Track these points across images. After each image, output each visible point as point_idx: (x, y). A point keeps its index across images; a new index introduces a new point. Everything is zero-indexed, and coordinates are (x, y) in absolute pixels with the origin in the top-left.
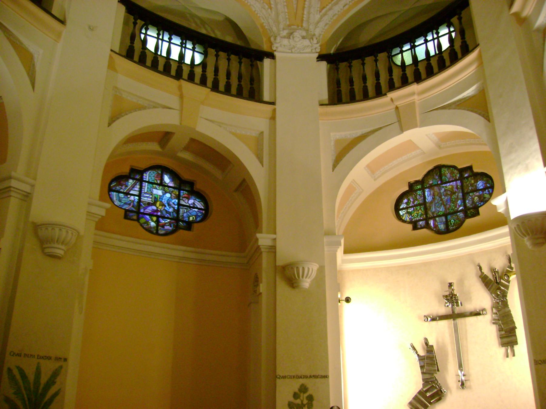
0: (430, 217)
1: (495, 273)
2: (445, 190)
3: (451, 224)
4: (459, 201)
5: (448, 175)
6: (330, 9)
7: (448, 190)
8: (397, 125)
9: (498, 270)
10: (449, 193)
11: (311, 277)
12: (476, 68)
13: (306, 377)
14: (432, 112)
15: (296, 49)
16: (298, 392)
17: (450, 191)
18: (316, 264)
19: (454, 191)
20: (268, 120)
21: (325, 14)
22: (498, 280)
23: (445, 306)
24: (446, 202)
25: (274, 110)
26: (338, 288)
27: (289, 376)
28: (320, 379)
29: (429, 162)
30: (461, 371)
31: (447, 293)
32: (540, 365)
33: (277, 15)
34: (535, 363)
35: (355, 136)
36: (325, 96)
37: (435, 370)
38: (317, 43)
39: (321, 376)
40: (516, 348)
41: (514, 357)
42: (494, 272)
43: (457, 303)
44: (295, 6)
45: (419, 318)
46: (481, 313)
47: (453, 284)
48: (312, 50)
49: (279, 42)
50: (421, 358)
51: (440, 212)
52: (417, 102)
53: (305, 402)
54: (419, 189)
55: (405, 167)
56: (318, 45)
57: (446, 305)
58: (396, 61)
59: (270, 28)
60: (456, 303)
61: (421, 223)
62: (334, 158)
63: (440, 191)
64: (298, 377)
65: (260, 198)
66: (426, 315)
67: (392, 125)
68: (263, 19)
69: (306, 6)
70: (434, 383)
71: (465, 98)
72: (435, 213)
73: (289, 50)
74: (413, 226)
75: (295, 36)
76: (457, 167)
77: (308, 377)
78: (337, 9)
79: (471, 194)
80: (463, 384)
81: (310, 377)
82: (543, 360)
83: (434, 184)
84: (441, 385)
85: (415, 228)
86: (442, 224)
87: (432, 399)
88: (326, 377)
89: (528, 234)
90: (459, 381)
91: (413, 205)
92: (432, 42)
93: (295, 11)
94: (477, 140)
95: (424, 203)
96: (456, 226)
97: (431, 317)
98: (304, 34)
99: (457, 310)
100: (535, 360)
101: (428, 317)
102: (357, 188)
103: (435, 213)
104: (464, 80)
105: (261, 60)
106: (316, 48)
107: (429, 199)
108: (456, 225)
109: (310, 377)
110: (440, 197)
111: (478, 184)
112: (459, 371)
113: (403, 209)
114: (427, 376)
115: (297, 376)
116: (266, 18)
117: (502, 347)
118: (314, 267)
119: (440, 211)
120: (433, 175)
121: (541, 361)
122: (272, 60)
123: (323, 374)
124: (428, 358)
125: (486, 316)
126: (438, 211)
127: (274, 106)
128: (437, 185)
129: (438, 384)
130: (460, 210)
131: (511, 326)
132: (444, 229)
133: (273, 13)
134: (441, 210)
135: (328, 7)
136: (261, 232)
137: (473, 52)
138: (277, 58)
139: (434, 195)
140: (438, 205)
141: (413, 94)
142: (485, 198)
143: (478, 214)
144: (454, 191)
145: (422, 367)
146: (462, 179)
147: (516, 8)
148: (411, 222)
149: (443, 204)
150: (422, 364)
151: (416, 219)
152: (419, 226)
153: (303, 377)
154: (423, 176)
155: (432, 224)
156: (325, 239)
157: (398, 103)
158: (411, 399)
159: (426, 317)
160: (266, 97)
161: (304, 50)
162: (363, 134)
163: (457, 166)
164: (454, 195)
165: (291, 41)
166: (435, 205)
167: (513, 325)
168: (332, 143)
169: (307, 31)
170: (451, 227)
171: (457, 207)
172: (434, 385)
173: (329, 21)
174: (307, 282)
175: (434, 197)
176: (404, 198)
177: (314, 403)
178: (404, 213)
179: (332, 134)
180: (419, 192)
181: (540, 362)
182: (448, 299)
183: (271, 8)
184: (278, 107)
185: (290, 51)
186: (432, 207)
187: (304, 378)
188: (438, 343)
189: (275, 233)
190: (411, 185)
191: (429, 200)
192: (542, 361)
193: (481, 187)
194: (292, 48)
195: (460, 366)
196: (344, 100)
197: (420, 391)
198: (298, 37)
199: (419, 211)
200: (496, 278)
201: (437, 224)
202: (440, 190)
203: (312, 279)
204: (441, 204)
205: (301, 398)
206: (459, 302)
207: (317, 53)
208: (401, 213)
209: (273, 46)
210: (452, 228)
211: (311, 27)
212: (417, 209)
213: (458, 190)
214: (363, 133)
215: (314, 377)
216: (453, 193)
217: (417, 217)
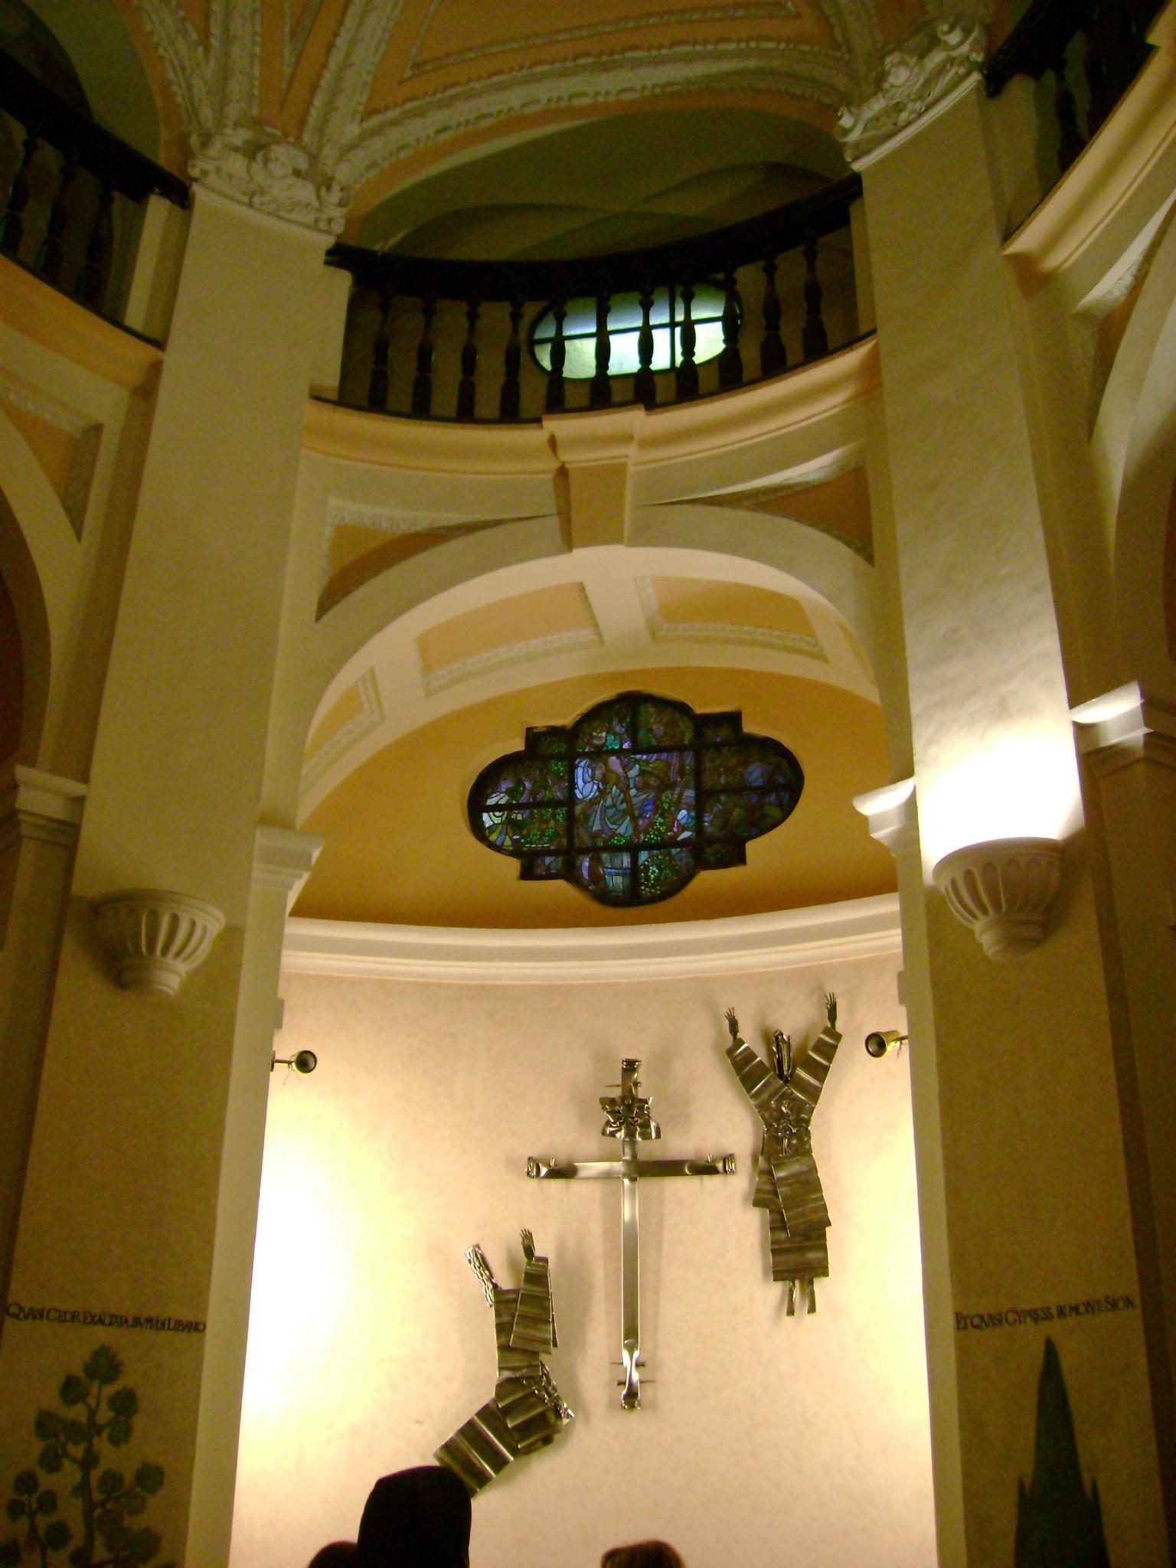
0: (584, 846)
1: (778, 1047)
2: (642, 773)
3: (648, 878)
4: (684, 812)
5: (659, 729)
6: (396, 123)
7: (651, 773)
8: (553, 523)
9: (789, 1038)
10: (652, 782)
11: (192, 958)
12: (847, 401)
13: (119, 1321)
14: (677, 507)
15: (266, 198)
16: (82, 1375)
17: (658, 777)
18: (220, 915)
19: (672, 780)
20: (126, 394)
21: (377, 132)
22: (785, 1067)
23: (604, 1133)
24: (639, 808)
25: (156, 368)
26: (274, 1017)
27: (57, 1310)
28: (174, 1332)
29: (612, 678)
30: (631, 1349)
31: (617, 1093)
32: (977, 1331)
33: (225, 73)
34: (958, 1322)
35: (404, 528)
36: (331, 379)
37: (545, 1342)
38: (341, 204)
39: (178, 1322)
40: (820, 1285)
41: (812, 1316)
42: (775, 1044)
43: (646, 1126)
44: (287, 70)
45: (511, 1163)
46: (720, 1166)
47: (638, 1066)
48: (316, 221)
49: (217, 159)
50: (502, 1300)
51: (617, 835)
52: (632, 469)
53: (105, 1415)
54: (560, 757)
55: (529, 679)
56: (338, 213)
57: (609, 1130)
58: (542, 360)
59: (192, 105)
60: (641, 1126)
61: (548, 860)
62: (325, 581)
63: (626, 773)
64: (89, 1319)
65: (47, 643)
66: (534, 1154)
67: (532, 522)
68: (175, 70)
69: (323, 83)
70: (536, 1383)
71: (790, 487)
72: (601, 837)
73: (244, 194)
74: (523, 866)
75: (273, 155)
76: (692, 709)
77: (126, 1321)
78: (419, 129)
79: (723, 798)
80: (631, 1397)
81: (137, 1321)
82: (989, 1315)
83: (610, 747)
84: (560, 1392)
85: (527, 873)
86: (617, 875)
87: (522, 1440)
88: (197, 1329)
89: (985, 911)
90: (621, 1383)
91: (531, 801)
92: (667, 331)
93: (284, 86)
94: (778, 633)
95: (571, 800)
96: (664, 888)
97: (552, 1164)
98: (303, 164)
99: (650, 1149)
100: (957, 1314)
101: (540, 1165)
102: (366, 705)
103: (601, 837)
104: (800, 430)
105: (139, 197)
106: (330, 221)
107: (585, 788)
108: (665, 885)
109: (137, 1321)
110: (625, 790)
111: (749, 770)
112: (625, 1354)
113: (496, 808)
114: (517, 1360)
115: (85, 1312)
116: (184, 69)
117: (776, 1279)
118: (211, 922)
119: (617, 832)
120: (610, 723)
121: (982, 1318)
122: (178, 209)
123: (186, 1315)
124: (528, 1298)
125: (731, 1179)
126: (610, 833)
127: (159, 353)
128: (618, 754)
129: (550, 1388)
130: (685, 839)
131: (814, 1217)
132: (624, 892)
133: (212, 63)
134: (621, 830)
135: (390, 115)
136: (32, 763)
137: (852, 350)
138: (198, 205)
139: (604, 780)
140: (614, 814)
141: (626, 438)
142: (765, 816)
143: (740, 859)
144: (669, 778)
145: (502, 1329)
146: (699, 747)
147: (1025, 241)
148: (516, 853)
149: (629, 811)
150: (505, 1319)
151: (534, 846)
152: (543, 869)
153: (107, 1320)
154: (579, 718)
155: (585, 873)
156: (262, 839)
157: (570, 457)
158: (450, 1434)
159: (535, 1162)
160: (136, 314)
161: (291, 211)
162: (432, 529)
163: (690, 704)
164: (668, 793)
165: (257, 167)
166: (603, 814)
167: (820, 1215)
168: (328, 532)
169: (314, 159)
170: (647, 890)
171: (675, 830)
172: (536, 1392)
173: (356, 182)
174: (176, 973)
175: (605, 789)
176: (504, 775)
177: (138, 1422)
178: (497, 821)
179: (333, 502)
180: (558, 767)
181: (977, 1321)
182: (619, 1112)
183: (207, 48)
184: (173, 359)
185: (246, 200)
186: (592, 819)
187: (110, 1324)
188: (560, 1257)
189: (84, 778)
190: (533, 737)
191: (585, 793)
192: (986, 1318)
193: (760, 782)
194: (253, 194)
195: (631, 1332)
196: (393, 402)
197: (486, 1407)
198: (283, 165)
199: (547, 822)
200: (780, 1061)
201: (602, 871)
202: (626, 767)
203: (197, 963)
204: (625, 813)
205: (92, 1401)
206: (653, 1124)
207: (329, 233)
208: (487, 819)
209: (190, 163)
210: (650, 892)
211: (329, 153)
212: (542, 816)
213: (684, 780)
214: (436, 525)
215: (149, 1325)
216: (666, 785)
217: (541, 839)
